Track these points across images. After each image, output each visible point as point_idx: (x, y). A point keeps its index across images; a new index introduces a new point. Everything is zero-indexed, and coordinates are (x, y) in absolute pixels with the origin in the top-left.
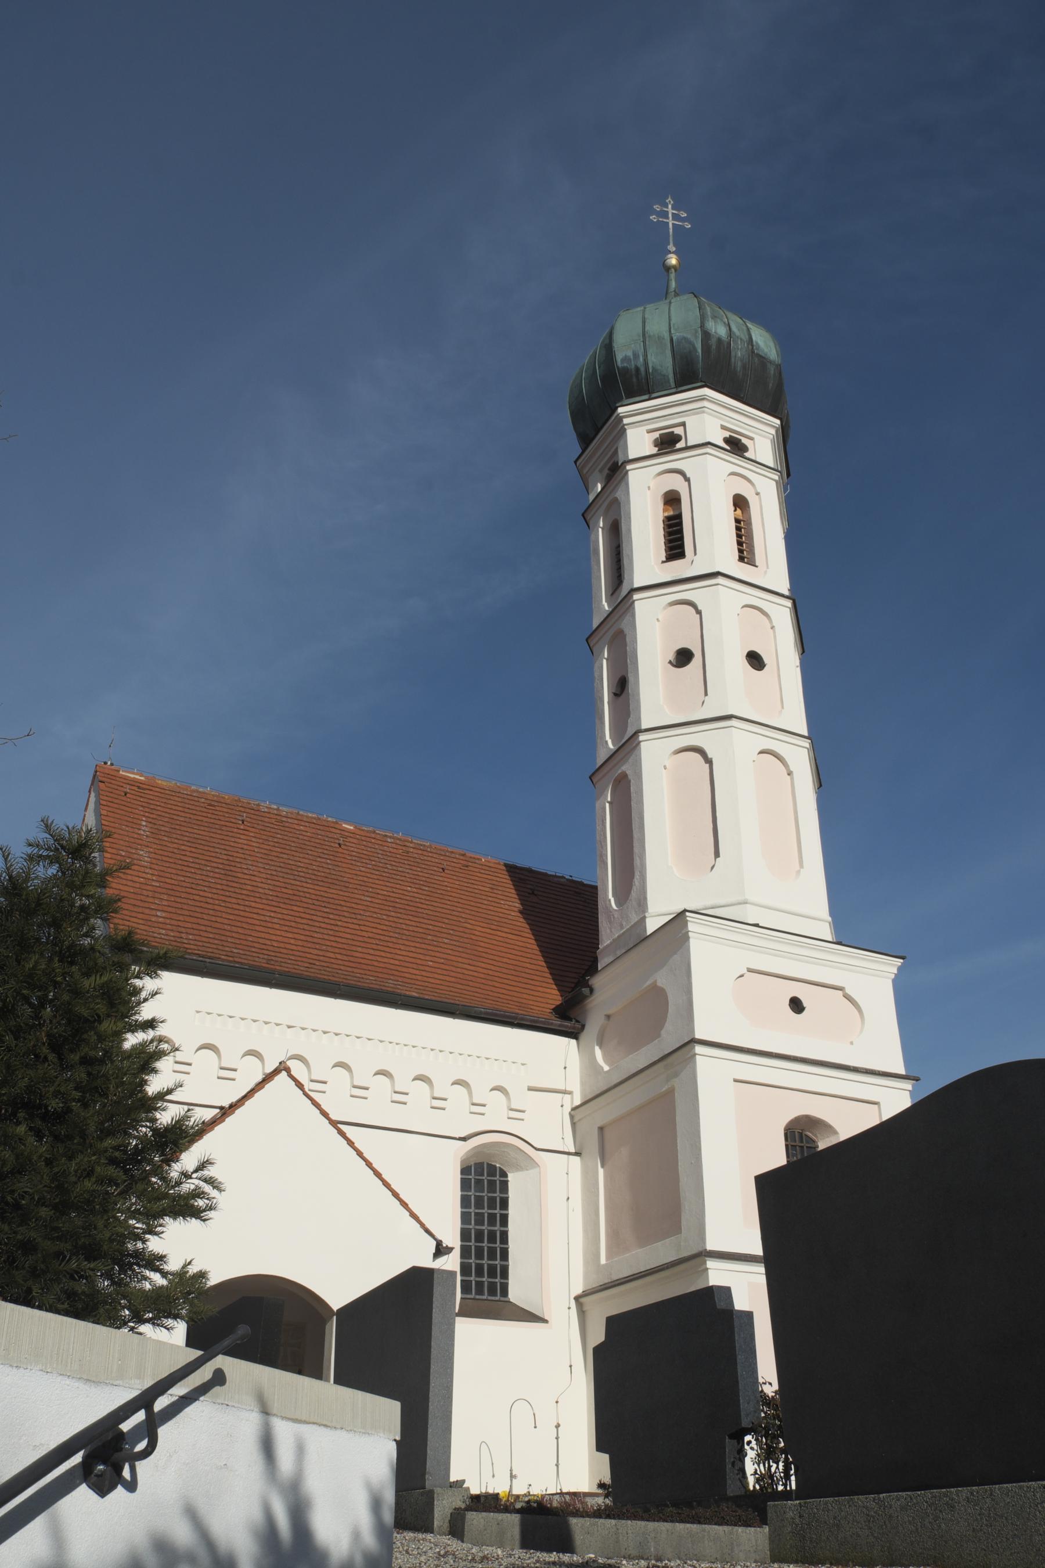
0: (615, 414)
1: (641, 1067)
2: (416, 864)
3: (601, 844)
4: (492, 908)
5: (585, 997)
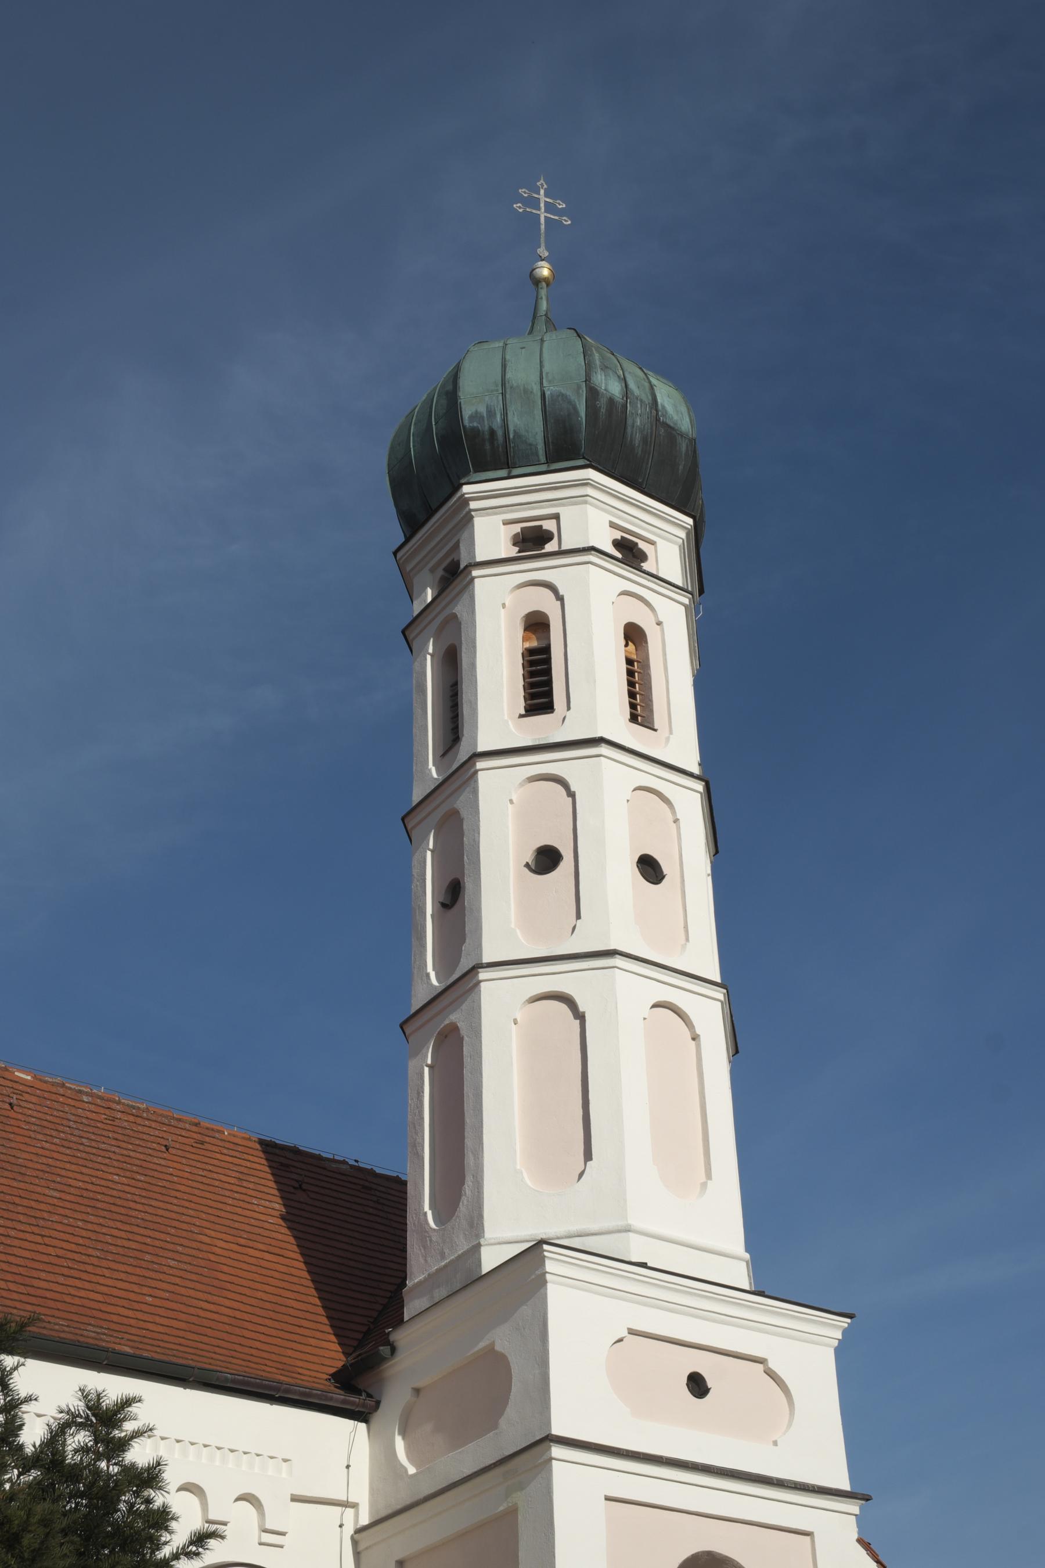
0: (458, 495)
1: (468, 1471)
2: (126, 1139)
3: (415, 1127)
4: (239, 1211)
5: (383, 1360)
